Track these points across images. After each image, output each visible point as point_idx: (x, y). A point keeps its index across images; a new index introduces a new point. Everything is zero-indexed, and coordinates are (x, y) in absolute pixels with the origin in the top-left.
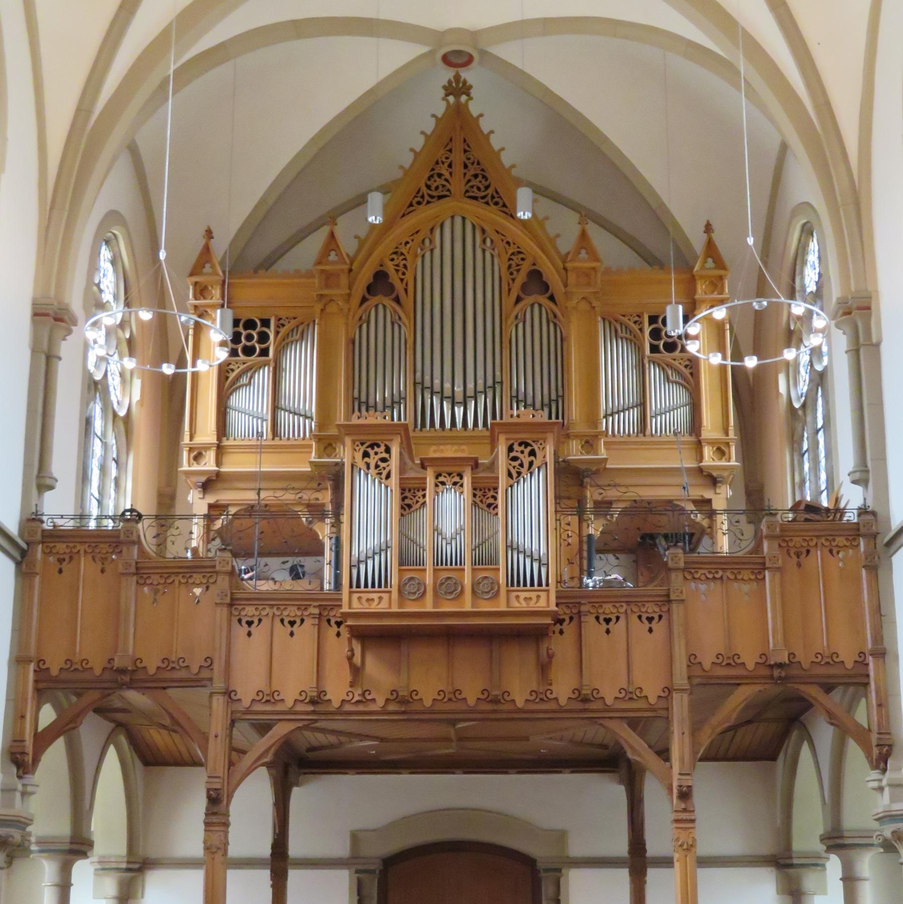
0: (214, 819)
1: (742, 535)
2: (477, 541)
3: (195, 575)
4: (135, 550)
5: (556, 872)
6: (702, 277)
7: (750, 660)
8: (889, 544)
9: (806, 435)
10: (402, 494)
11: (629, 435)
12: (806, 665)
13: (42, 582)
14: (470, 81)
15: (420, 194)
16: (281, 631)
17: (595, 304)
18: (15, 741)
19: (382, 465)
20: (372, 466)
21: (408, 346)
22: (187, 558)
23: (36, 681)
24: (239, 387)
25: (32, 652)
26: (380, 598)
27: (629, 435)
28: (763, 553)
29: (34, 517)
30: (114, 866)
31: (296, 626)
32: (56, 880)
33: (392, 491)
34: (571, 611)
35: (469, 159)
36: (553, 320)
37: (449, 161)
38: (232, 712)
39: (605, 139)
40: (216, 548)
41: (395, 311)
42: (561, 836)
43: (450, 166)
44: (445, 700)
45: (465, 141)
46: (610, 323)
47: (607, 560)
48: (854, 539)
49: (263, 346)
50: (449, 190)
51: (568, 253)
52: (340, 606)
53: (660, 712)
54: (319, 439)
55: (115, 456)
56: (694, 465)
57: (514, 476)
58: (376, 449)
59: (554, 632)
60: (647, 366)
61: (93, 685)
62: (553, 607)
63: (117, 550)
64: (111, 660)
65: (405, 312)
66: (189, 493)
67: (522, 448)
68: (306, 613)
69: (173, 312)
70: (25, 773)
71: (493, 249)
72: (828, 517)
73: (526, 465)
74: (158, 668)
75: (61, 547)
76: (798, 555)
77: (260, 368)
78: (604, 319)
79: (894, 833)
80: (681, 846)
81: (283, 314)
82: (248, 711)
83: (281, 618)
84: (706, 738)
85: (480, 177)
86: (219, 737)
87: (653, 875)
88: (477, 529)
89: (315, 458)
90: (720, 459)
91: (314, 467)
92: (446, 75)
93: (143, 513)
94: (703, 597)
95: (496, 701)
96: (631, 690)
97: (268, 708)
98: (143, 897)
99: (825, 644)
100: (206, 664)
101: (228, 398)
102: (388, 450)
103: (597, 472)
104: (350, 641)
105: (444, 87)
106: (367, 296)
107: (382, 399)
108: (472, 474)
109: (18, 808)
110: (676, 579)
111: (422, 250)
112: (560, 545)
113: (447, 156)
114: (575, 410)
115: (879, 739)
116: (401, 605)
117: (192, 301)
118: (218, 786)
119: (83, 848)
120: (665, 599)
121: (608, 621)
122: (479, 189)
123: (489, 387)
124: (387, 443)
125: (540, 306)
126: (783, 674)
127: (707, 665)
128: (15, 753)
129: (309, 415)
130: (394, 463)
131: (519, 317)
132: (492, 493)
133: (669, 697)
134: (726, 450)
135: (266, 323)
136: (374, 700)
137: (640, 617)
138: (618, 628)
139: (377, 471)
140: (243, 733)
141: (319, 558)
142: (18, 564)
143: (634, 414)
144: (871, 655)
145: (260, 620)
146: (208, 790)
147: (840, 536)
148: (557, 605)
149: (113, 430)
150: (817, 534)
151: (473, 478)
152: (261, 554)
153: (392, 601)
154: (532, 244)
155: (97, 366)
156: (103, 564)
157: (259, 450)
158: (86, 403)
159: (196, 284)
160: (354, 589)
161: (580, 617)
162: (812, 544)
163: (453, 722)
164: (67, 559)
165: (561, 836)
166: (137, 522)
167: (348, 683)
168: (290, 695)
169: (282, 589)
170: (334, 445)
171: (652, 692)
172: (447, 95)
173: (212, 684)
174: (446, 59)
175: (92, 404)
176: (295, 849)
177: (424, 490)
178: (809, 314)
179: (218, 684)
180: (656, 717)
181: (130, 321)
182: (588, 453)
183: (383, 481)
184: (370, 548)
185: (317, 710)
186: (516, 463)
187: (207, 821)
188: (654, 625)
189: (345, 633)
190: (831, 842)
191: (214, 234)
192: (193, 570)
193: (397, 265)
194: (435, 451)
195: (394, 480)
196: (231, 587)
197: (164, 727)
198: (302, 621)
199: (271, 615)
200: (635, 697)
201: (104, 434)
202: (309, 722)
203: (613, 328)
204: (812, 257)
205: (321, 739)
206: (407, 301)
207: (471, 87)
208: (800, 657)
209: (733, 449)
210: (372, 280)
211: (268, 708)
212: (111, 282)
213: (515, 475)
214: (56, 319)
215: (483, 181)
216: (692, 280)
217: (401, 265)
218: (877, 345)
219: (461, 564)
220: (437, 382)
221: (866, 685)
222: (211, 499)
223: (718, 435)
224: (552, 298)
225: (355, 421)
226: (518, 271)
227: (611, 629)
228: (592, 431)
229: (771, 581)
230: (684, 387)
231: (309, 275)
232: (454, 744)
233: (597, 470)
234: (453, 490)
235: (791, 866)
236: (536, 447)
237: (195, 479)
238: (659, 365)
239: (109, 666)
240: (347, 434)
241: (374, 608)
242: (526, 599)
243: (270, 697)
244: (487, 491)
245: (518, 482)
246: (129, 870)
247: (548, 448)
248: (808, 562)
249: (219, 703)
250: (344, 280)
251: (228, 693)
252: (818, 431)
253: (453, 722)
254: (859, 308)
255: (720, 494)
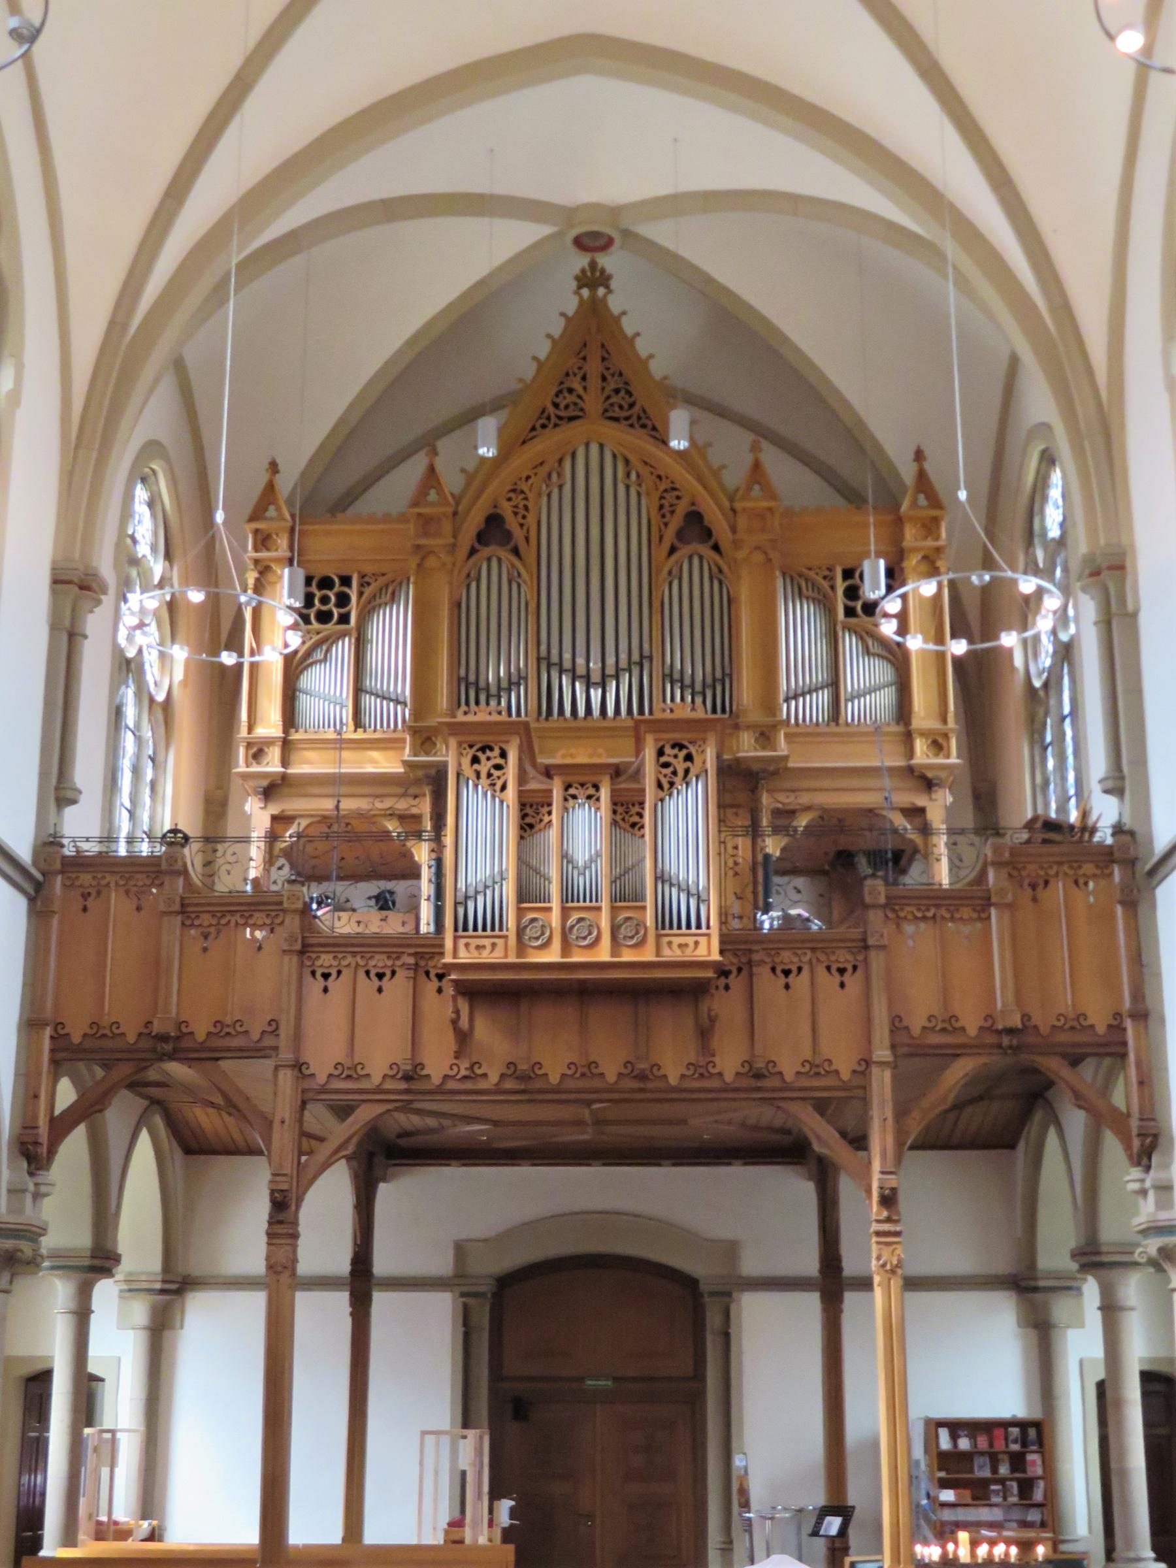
0: (280, 1229)
1: (961, 860)
2: (618, 870)
3: (257, 915)
4: (180, 882)
5: (727, 1292)
6: (911, 519)
7: (972, 1025)
8: (1152, 873)
9: (1049, 721)
10: (521, 810)
11: (817, 724)
12: (1044, 1030)
13: (61, 923)
14: (610, 269)
15: (545, 415)
16: (367, 986)
17: (773, 554)
18: (25, 1128)
19: (496, 773)
20: (483, 775)
21: (530, 608)
22: (246, 892)
23: (53, 1051)
24: (311, 665)
25: (48, 1013)
26: (494, 945)
27: (817, 724)
28: (987, 884)
29: (52, 840)
30: (145, 1286)
31: (386, 979)
32: (73, 1305)
33: (508, 806)
34: (740, 961)
35: (608, 369)
36: (718, 575)
37: (582, 372)
38: (303, 1091)
39: (785, 340)
40: (283, 879)
41: (513, 566)
42: (731, 1250)
43: (584, 378)
44: (578, 1075)
45: (603, 346)
46: (792, 579)
47: (786, 893)
48: (1107, 867)
49: (343, 611)
50: (582, 410)
51: (737, 490)
52: (442, 954)
53: (855, 1091)
54: (415, 731)
55: (151, 752)
56: (900, 762)
57: (665, 787)
58: (488, 753)
59: (717, 988)
60: (840, 634)
61: (125, 1056)
62: (716, 956)
63: (157, 882)
64: (149, 1023)
65: (525, 566)
66: (246, 801)
67: (676, 751)
68: (399, 963)
69: (233, 592)
70: (38, 1169)
71: (640, 485)
72: (1073, 836)
73: (681, 773)
74: (209, 1033)
75: (86, 878)
76: (1033, 887)
77: (338, 639)
78: (784, 574)
79: (1161, 1250)
80: (883, 1266)
81: (368, 569)
82: (323, 1090)
83: (366, 969)
84: (915, 1128)
85: (622, 393)
86: (287, 1123)
87: (851, 1299)
88: (616, 853)
89: (409, 756)
90: (936, 755)
91: (408, 769)
92: (580, 261)
93: (190, 834)
94: (910, 943)
95: (642, 1077)
96: (817, 1062)
97: (350, 1085)
98: (182, 1327)
99: (1070, 1002)
100: (270, 1029)
101: (298, 678)
102: (503, 755)
103: (775, 773)
104: (454, 998)
105: (577, 278)
106: (477, 546)
107: (496, 680)
108: (612, 784)
109: (29, 1214)
110: (875, 918)
111: (547, 486)
112: (726, 874)
113: (579, 365)
114: (746, 693)
115: (1140, 1127)
116: (519, 955)
117: (251, 553)
118: (285, 1187)
119: (107, 1264)
120: (862, 944)
121: (787, 973)
122: (621, 407)
123: (635, 663)
124: (504, 746)
125: (701, 558)
126: (1015, 1042)
127: (916, 1031)
128: (26, 1143)
129: (401, 699)
130: (511, 773)
131: (674, 572)
132: (637, 809)
133: (867, 1072)
134: (944, 744)
135: (346, 581)
136: (485, 1075)
137: (828, 968)
138: (801, 983)
139: (489, 781)
140: (318, 1117)
141: (414, 882)
142: (32, 900)
143: (824, 697)
144: (1130, 1016)
145: (339, 972)
146: (272, 1192)
147: (1087, 861)
148: (722, 952)
149: (150, 720)
150: (1058, 859)
151: (613, 791)
152: (340, 878)
153: (509, 948)
154: (688, 476)
155: (130, 639)
156: (139, 899)
157: (338, 746)
158: (115, 687)
159: (256, 532)
160: (461, 933)
161: (751, 967)
162: (1052, 872)
163: (589, 1103)
164: (94, 894)
165: (731, 1250)
166: (183, 846)
167: (452, 1054)
168: (377, 1068)
169: (367, 932)
170: (434, 739)
171: (845, 1066)
172: (580, 287)
173: (277, 1055)
174: (579, 242)
175: (123, 688)
176: (382, 1265)
177: (550, 805)
178: (1040, 592)
179: (286, 1055)
180: (852, 1097)
181: (171, 579)
182: (764, 748)
183: (498, 794)
184: (481, 880)
185: (413, 1087)
186: (668, 771)
187: (270, 1231)
188: (847, 977)
189: (450, 991)
190: (1085, 1259)
191: (281, 467)
192: (253, 908)
193: (516, 507)
194: (564, 756)
195: (511, 793)
196: (302, 931)
197: (212, 1104)
198: (393, 973)
199: (353, 965)
200: (823, 1072)
201: (138, 724)
202: (405, 1103)
203: (795, 583)
204: (1055, 495)
205: (416, 1121)
206: (529, 554)
207: (609, 277)
208: (1037, 1019)
209: (953, 742)
210: (483, 526)
211: (350, 1085)
212: (148, 530)
213: (666, 786)
214: (82, 588)
215: (627, 397)
216: (899, 522)
217: (521, 506)
218: (1134, 615)
219: (597, 901)
220: (567, 656)
221: (1124, 1056)
222: (274, 809)
223: (933, 724)
224: (716, 548)
225: (461, 718)
226: (672, 512)
227: (791, 984)
228: (769, 720)
229: (1000, 919)
230: (889, 661)
231: (403, 518)
232: (590, 1129)
233: (774, 772)
234: (587, 805)
235: (1036, 1289)
236: (693, 749)
237: (252, 783)
238: (856, 633)
239: (146, 1031)
240: (452, 734)
241: (487, 957)
242: (680, 946)
243: (351, 1071)
244: (630, 806)
245: (670, 795)
246: (163, 1291)
247: (709, 751)
248: (1044, 895)
249: (286, 1078)
250: (447, 526)
251: (299, 1066)
252: (1063, 718)
253: (589, 1103)
254: (1110, 568)
255: (936, 800)
